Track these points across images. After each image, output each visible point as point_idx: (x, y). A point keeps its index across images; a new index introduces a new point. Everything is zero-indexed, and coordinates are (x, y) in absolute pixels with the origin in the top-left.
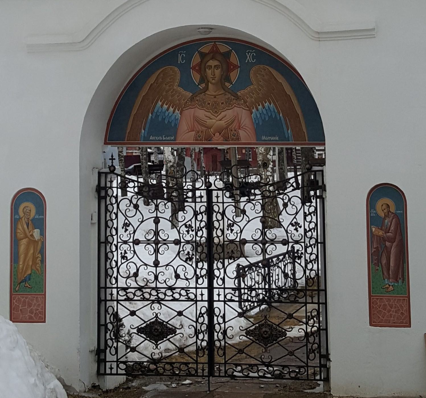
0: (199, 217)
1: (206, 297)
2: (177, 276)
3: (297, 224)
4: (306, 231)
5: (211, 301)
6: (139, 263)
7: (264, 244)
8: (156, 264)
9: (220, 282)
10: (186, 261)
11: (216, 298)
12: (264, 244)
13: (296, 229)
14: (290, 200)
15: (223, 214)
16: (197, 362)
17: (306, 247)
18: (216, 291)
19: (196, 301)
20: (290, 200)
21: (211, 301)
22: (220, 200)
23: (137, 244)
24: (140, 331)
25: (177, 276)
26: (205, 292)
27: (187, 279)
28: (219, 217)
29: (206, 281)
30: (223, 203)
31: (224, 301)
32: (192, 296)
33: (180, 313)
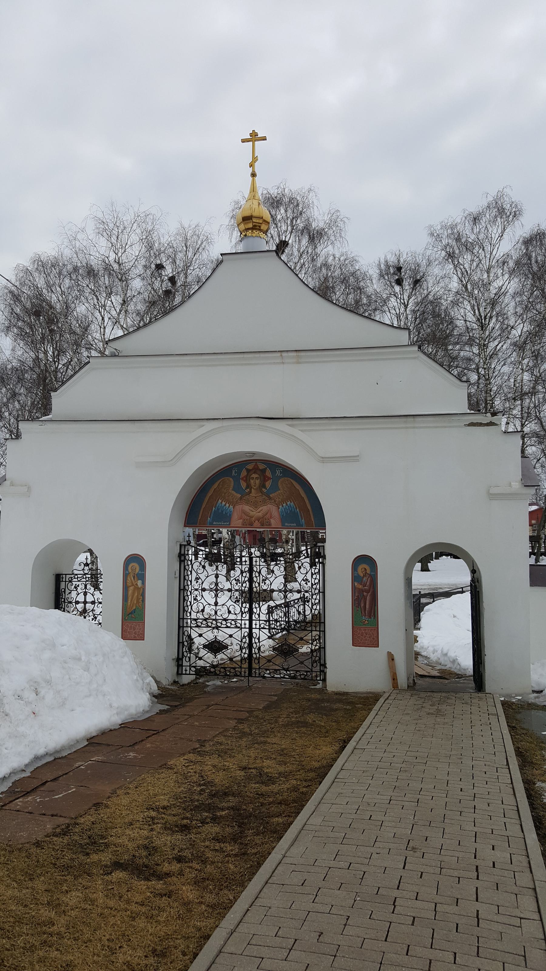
0: (244, 574)
1: (247, 626)
2: (229, 612)
3: (307, 580)
4: (312, 585)
5: (251, 628)
6: (205, 603)
7: (285, 593)
8: (216, 604)
9: (257, 616)
10: (235, 603)
11: (254, 626)
12: (285, 593)
13: (306, 583)
14: (302, 564)
15: (260, 573)
16: (241, 667)
17: (312, 595)
18: (254, 622)
19: (241, 628)
20: (302, 564)
21: (251, 628)
22: (258, 564)
23: (204, 591)
24: (205, 646)
25: (229, 612)
26: (247, 622)
27: (236, 614)
28: (257, 575)
29: (248, 615)
30: (260, 565)
31: (259, 629)
32: (239, 625)
33: (231, 636)
